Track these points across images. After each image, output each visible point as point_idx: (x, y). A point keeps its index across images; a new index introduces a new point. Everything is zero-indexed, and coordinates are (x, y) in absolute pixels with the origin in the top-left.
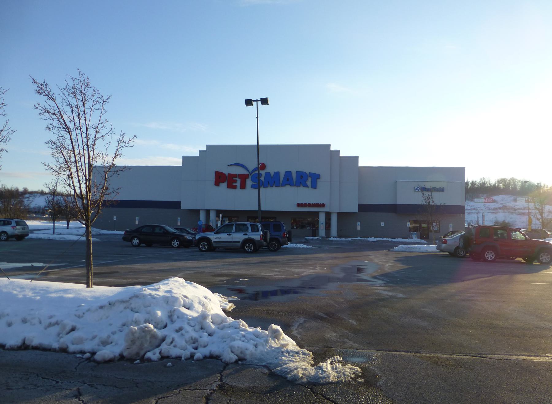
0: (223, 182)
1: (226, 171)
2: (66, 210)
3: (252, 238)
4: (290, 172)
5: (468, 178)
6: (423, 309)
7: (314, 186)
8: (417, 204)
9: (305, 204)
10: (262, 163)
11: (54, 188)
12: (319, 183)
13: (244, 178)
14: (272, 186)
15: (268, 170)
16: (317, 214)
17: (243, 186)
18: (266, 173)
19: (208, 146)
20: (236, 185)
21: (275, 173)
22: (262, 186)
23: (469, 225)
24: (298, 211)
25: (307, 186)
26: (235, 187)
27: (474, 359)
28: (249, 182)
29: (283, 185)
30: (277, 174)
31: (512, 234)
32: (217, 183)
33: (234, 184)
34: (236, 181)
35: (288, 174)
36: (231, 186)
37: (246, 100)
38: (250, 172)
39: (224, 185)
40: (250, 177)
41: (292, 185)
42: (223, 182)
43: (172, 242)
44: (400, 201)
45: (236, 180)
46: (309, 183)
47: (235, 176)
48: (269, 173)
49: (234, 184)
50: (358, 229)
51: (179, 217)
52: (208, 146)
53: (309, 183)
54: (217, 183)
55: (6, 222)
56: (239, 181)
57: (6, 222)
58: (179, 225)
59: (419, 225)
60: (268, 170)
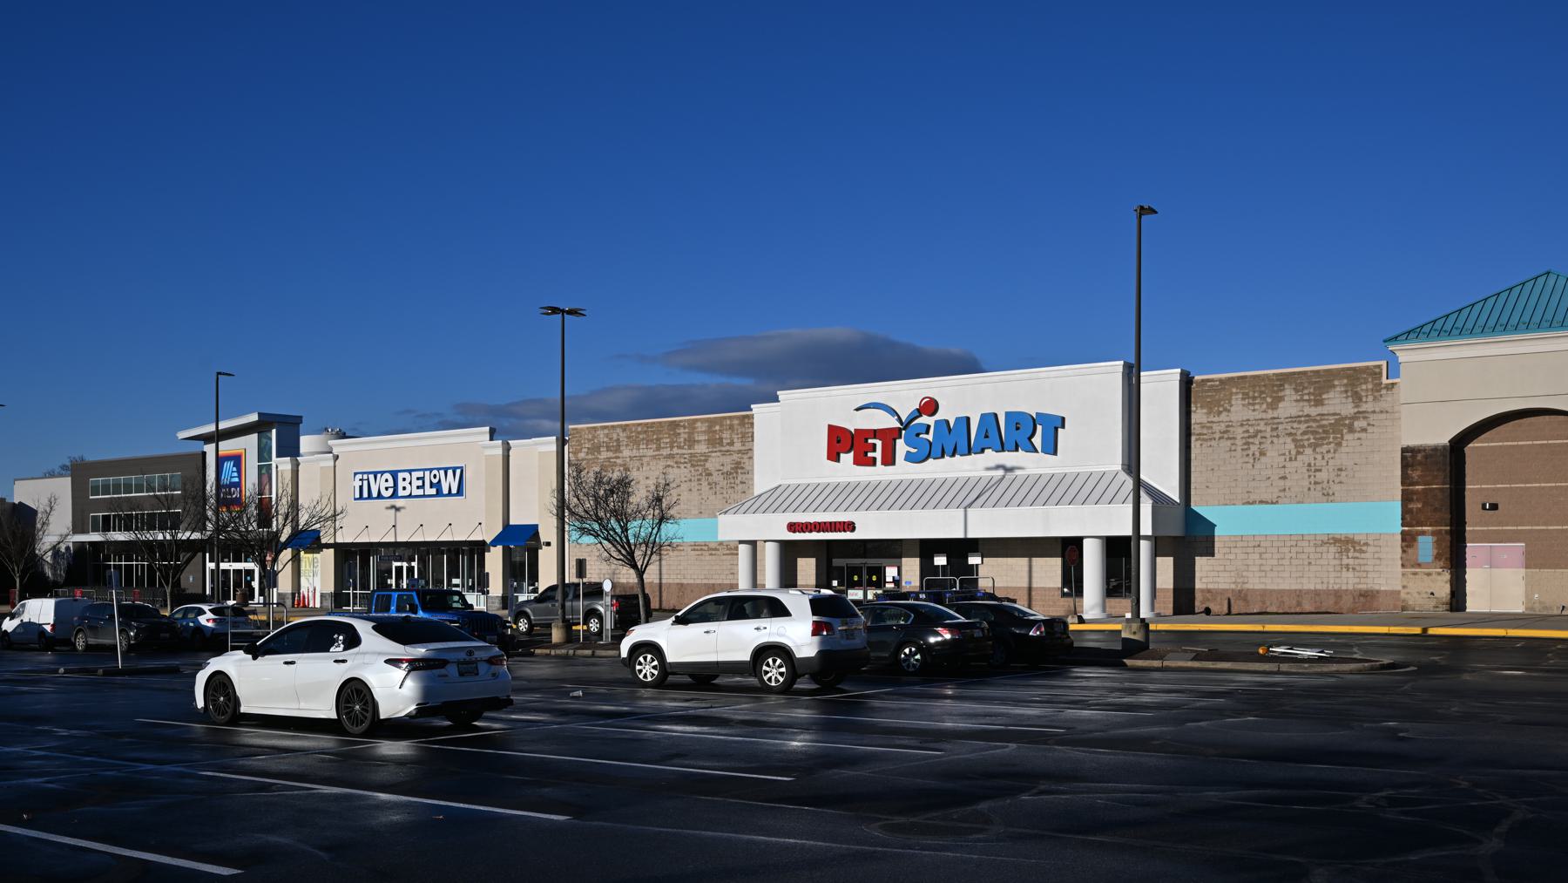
2: (235, 523)
5: (387, 508)
6: (241, 762)
7: (1052, 448)
11: (1312, 403)
13: (889, 437)
16: (861, 568)
17: (889, 460)
19: (776, 399)
24: (1005, 559)
26: (873, 462)
28: (901, 447)
32: (834, 456)
35: (990, 419)
36: (863, 460)
39: (847, 458)
44: (1141, 505)
45: (874, 445)
52: (776, 399)
54: (834, 456)
57: (635, 602)
59: (91, 497)
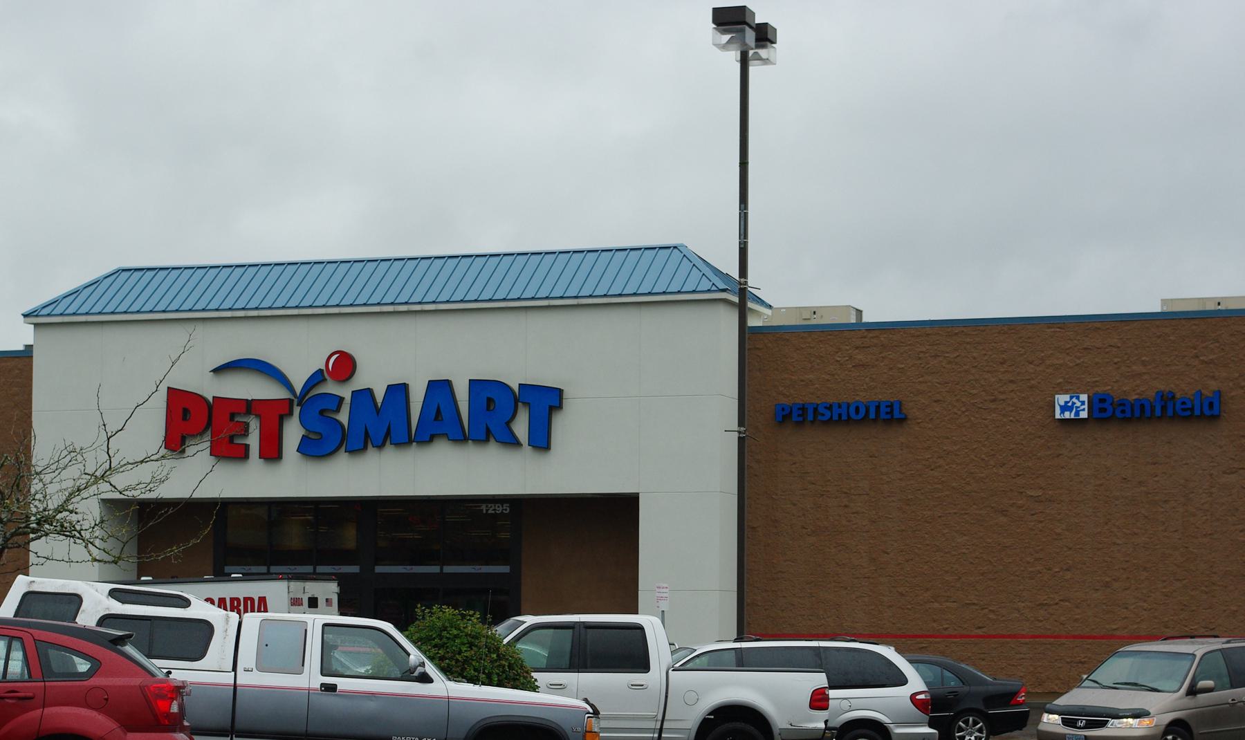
1: (212, 389)
4: (447, 384)
7: (541, 441)
8: (640, 587)
9: (1166, 399)
12: (562, 426)
14: (380, 446)
15: (361, 381)
18: (353, 392)
20: (472, 382)
21: (391, 388)
22: (343, 448)
25: (514, 442)
28: (293, 432)
30: (399, 391)
37: (715, 10)
38: (298, 391)
41: (461, 437)
43: (983, 722)
46: (521, 427)
48: (369, 392)
51: (224, 570)
53: (521, 427)
58: (508, 567)
60: (361, 381)
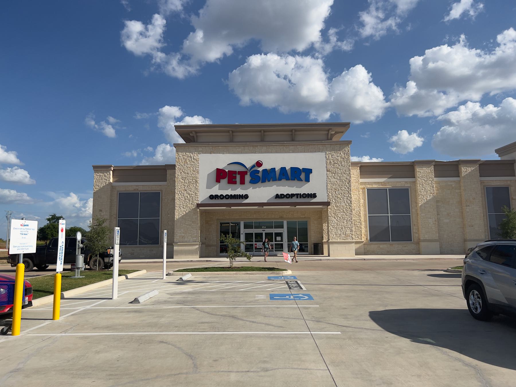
0: (224, 178)
3: (478, 279)
7: (307, 180)
10: (262, 162)
13: (243, 174)
17: (242, 182)
23: (160, 59)
26: (235, 183)
27: (35, 279)
28: (248, 178)
29: (280, 179)
31: (362, 136)
32: (218, 181)
33: (234, 180)
34: (235, 177)
35: (283, 169)
39: (224, 181)
40: (249, 174)
42: (224, 178)
47: (235, 172)
49: (234, 180)
50: (149, 147)
55: (224, 248)
56: (238, 177)
57: (224, 248)
